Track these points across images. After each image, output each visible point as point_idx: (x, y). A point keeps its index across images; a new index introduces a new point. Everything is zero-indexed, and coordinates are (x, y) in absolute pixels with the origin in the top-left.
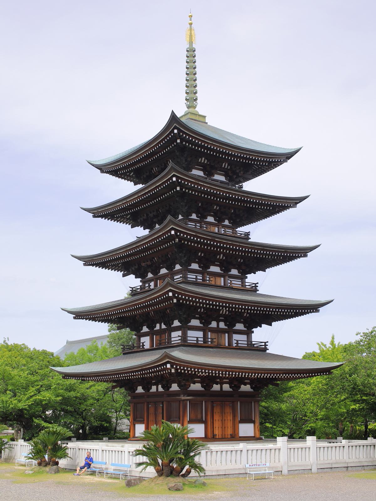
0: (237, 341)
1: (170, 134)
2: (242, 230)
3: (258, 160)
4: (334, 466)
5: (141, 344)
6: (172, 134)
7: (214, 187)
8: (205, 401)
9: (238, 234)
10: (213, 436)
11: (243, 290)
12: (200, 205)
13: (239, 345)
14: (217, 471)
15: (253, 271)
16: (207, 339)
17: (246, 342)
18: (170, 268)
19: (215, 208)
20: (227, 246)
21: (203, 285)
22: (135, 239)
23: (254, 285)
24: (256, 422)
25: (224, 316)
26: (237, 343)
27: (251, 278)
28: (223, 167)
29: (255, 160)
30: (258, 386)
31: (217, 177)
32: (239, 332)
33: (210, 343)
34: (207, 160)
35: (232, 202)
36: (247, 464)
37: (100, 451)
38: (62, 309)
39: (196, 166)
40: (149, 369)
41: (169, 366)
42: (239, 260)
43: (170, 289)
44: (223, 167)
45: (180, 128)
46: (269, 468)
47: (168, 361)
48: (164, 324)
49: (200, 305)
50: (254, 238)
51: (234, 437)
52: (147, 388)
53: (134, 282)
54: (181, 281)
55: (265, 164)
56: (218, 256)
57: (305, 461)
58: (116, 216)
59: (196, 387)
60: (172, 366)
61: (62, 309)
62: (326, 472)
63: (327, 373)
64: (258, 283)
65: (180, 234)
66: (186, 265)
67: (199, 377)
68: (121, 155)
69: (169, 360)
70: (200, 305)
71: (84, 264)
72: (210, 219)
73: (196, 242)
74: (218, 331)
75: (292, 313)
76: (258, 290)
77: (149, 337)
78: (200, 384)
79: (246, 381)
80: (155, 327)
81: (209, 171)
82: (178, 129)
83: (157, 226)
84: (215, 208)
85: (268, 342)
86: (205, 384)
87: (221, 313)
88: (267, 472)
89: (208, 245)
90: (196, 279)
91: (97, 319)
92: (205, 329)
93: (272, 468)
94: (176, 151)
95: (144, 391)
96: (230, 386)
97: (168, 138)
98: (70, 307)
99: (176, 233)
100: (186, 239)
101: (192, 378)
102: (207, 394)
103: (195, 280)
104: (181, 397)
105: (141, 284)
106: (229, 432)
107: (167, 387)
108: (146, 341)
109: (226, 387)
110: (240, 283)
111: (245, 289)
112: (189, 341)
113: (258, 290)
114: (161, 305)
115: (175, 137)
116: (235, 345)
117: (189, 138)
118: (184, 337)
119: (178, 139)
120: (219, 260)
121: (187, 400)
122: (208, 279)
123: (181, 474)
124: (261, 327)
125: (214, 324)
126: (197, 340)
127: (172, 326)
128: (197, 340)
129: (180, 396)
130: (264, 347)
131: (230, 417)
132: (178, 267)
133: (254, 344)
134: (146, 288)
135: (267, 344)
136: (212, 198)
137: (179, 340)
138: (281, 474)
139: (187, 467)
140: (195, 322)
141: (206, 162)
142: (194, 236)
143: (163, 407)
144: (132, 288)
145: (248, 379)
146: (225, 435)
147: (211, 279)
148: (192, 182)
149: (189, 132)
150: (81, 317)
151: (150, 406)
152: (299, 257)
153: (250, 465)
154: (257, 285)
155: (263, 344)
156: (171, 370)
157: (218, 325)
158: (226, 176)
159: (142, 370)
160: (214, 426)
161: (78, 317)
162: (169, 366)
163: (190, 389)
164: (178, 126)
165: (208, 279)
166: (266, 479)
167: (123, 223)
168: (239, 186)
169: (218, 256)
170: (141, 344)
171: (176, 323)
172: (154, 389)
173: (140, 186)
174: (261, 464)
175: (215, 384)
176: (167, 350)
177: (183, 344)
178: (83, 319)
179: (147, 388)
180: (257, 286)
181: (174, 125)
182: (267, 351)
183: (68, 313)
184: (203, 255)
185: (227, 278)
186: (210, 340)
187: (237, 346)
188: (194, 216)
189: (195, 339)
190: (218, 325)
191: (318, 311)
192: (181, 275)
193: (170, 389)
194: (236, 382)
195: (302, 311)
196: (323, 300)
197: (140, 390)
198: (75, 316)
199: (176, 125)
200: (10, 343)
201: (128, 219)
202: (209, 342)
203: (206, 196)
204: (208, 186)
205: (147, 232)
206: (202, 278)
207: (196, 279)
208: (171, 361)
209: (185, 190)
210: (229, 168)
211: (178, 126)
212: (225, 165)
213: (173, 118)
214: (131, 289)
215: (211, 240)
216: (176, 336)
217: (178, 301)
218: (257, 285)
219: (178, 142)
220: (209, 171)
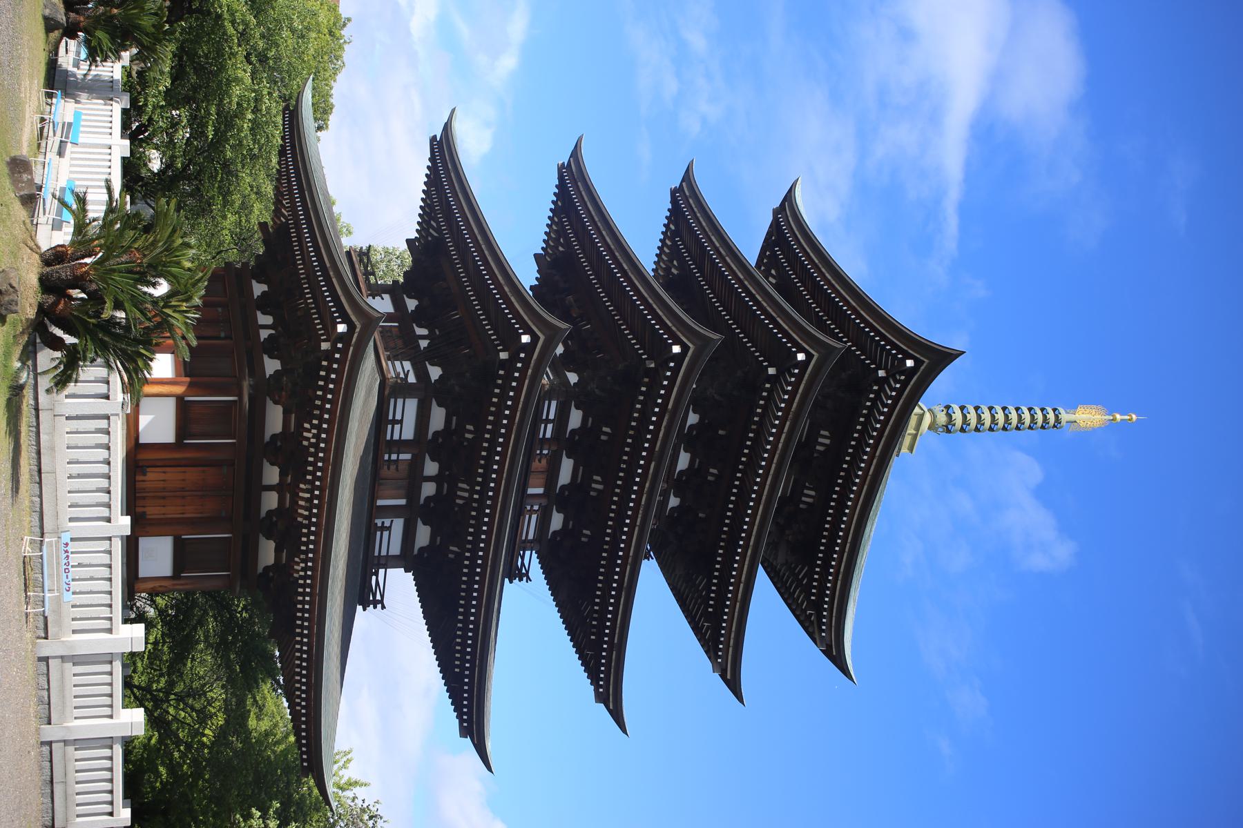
0: (389, 528)
4: (58, 789)
7: (775, 461)
8: (235, 443)
10: (142, 467)
11: (517, 546)
14: (53, 449)
16: (395, 449)
17: (384, 553)
24: (175, 582)
25: (452, 494)
26: (383, 528)
32: (409, 535)
34: (826, 449)
36: (72, 540)
42: (588, 532)
43: (539, 338)
45: (919, 374)
46: (58, 600)
51: (142, 525)
52: (264, 304)
56: (598, 478)
57: (74, 705)
60: (341, 337)
62: (41, 768)
63: (305, 764)
65: (670, 369)
69: (358, 330)
72: (684, 460)
74: (415, 477)
76: (511, 582)
78: (281, 430)
80: (420, 326)
82: (913, 371)
85: (383, 607)
86: (279, 444)
88: (48, 595)
90: (547, 421)
92: (422, 443)
93: (58, 611)
94: (850, 372)
103: (544, 417)
104: (247, 378)
106: (153, 511)
107: (271, 347)
109: (271, 501)
111: (517, 546)
112: (392, 401)
113: (511, 582)
116: (379, 522)
120: (588, 479)
121: (240, 395)
122: (545, 452)
123: (47, 321)
125: (431, 468)
126: (394, 422)
128: (394, 422)
129: (250, 376)
131: (191, 512)
135: (379, 606)
136: (744, 459)
138: (39, 638)
139: (70, 340)
141: (818, 448)
143: (218, 338)
146: (144, 498)
151: (220, 310)
152: (459, 717)
153: (67, 544)
155: (378, 597)
157: (429, 479)
160: (168, 469)
164: (922, 368)
165: (545, 452)
166: (26, 591)
169: (598, 478)
172: (264, 319)
174: (70, 578)
181: (925, 360)
182: (361, 606)
183: (446, 124)
185: (544, 502)
186: (394, 457)
187: (376, 528)
189: (398, 417)
190: (429, 479)
198: (438, 140)
199: (925, 365)
202: (390, 457)
204: (780, 445)
207: (547, 421)
208: (356, 335)
210: (801, 506)
211: (924, 370)
215: (650, 450)
216: (404, 369)
217: (503, 364)
219: (907, 361)
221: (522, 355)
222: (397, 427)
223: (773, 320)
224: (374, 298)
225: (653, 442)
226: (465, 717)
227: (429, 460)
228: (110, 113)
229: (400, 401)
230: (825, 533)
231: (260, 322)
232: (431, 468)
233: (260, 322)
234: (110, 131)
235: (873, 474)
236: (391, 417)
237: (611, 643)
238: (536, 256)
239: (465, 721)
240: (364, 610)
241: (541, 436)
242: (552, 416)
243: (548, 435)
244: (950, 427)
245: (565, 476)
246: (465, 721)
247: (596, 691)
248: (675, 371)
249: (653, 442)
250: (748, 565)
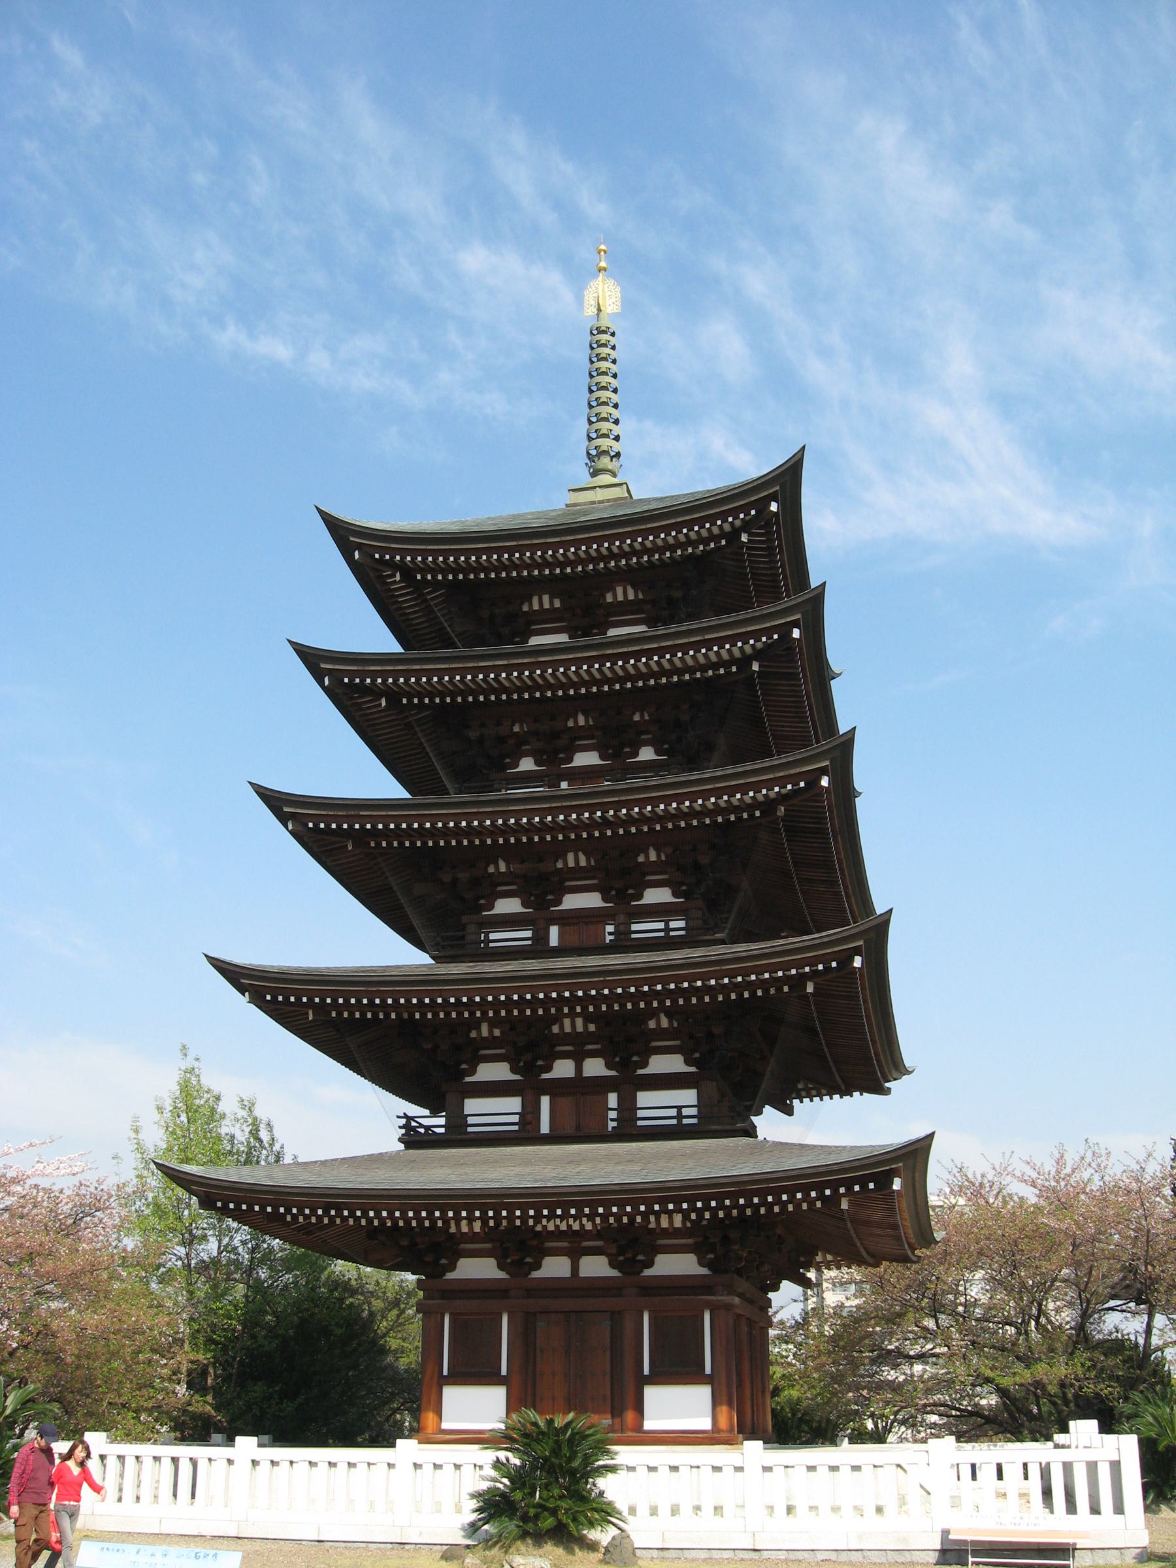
70: (649, 1004)
74: (580, 1086)
90: (667, 929)
96: (698, 1259)
103: (662, 934)
126: (680, 1116)
128: (680, 1116)
141: (631, 597)
149: (703, 511)
193: (447, 1274)
200: (300, 1160)
207: (667, 929)
222: (685, 1112)
227: (551, 1073)
229: (470, 1120)
232: (563, 1069)
235: (515, 541)
236: (674, 1122)
241: (529, 942)
242: (661, 925)
243: (682, 924)
244: (612, 454)
245: (592, 900)
250: (745, 627)
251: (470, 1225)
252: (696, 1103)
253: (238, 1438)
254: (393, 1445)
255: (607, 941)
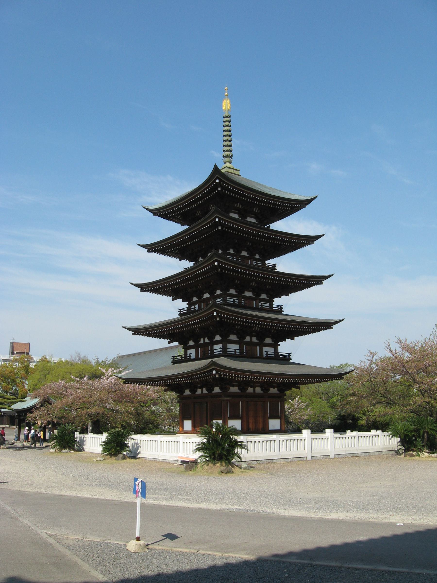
0: (267, 352)
1: (213, 183)
2: (270, 262)
3: (283, 206)
5: (188, 355)
6: (215, 184)
9: (267, 266)
11: (271, 310)
12: (236, 242)
13: (269, 355)
15: (279, 296)
17: (273, 354)
18: (212, 293)
19: (248, 244)
20: (259, 275)
21: (239, 306)
22: (183, 270)
23: (279, 307)
26: (267, 354)
27: (277, 302)
28: (254, 211)
29: (280, 205)
30: (283, 389)
31: (249, 219)
33: (245, 354)
35: (262, 240)
37: (159, 442)
38: (123, 327)
39: (233, 210)
40: (197, 375)
41: (214, 372)
43: (215, 309)
44: (254, 211)
45: (221, 178)
47: (214, 368)
48: (208, 339)
49: (238, 322)
50: (279, 269)
51: (265, 431)
52: (193, 391)
53: (182, 304)
54: (222, 303)
55: (289, 209)
58: (167, 251)
59: (234, 389)
60: (217, 372)
61: (123, 327)
64: (283, 306)
66: (225, 290)
67: (236, 382)
68: (171, 201)
69: (215, 367)
70: (238, 322)
71: (140, 290)
72: (244, 253)
73: (235, 271)
74: (251, 344)
75: (311, 329)
76: (283, 311)
77: (194, 350)
79: (274, 385)
80: (200, 341)
81: (243, 214)
83: (201, 259)
84: (248, 244)
85: (291, 353)
87: (254, 329)
89: (243, 273)
90: (234, 301)
91: (152, 335)
92: (240, 342)
95: (221, 391)
97: (206, 191)
98: (129, 326)
99: (219, 264)
100: (227, 269)
101: (230, 382)
102: (243, 395)
103: (233, 302)
105: (187, 306)
106: (260, 426)
107: (210, 390)
108: (192, 352)
109: (258, 390)
110: (268, 305)
112: (228, 352)
113: (283, 311)
114: (202, 324)
115: (217, 185)
116: (265, 356)
117: (228, 187)
118: (225, 349)
119: (219, 187)
121: (227, 400)
124: (285, 341)
125: (248, 339)
126: (235, 352)
127: (215, 340)
128: (235, 352)
130: (288, 357)
132: (218, 292)
133: (281, 355)
134: (192, 310)
135: (290, 354)
137: (221, 351)
140: (233, 337)
141: (240, 207)
142: (233, 266)
143: (207, 406)
144: (180, 310)
145: (276, 383)
147: (246, 302)
148: (231, 223)
150: (139, 334)
151: (196, 405)
152: (316, 284)
154: (282, 307)
155: (287, 355)
156: (215, 375)
157: (251, 339)
158: (256, 218)
159: (192, 376)
161: (136, 334)
162: (214, 372)
163: (230, 391)
167: (172, 257)
168: (267, 226)
170: (188, 355)
171: (218, 338)
172: (199, 391)
173: (186, 227)
175: (231, 387)
176: (214, 360)
177: (224, 354)
178: (140, 335)
179: (193, 391)
180: (283, 308)
184: (239, 282)
185: (258, 300)
186: (245, 351)
188: (231, 251)
189: (234, 350)
190: (251, 339)
191: (332, 328)
192: (222, 299)
194: (266, 386)
195: (319, 328)
196: (336, 319)
197: (187, 392)
198: (133, 332)
201: (176, 254)
202: (245, 353)
203: (242, 234)
205: (192, 264)
206: (238, 301)
207: (234, 301)
208: (217, 368)
209: (225, 229)
212: (256, 210)
213: (216, 170)
214: (179, 311)
215: (247, 270)
216: (218, 348)
217: (221, 319)
218: (282, 307)
220: (243, 214)
221: (220, 314)
223: (203, 226)
224: (191, 356)
225: (244, 269)
226: (317, 283)
228: (93, 438)
230: (269, 206)
231: (200, 393)
233: (200, 393)
234: (101, 438)
236: (234, 353)
237: (305, 280)
238: (173, 299)
239: (318, 283)
240: (291, 359)
246: (318, 283)
247: (310, 244)
248: (223, 263)
249: (244, 269)
251: (240, 379)
252: (239, 349)
253: (372, 430)
254: (370, 431)
255: (260, 307)
